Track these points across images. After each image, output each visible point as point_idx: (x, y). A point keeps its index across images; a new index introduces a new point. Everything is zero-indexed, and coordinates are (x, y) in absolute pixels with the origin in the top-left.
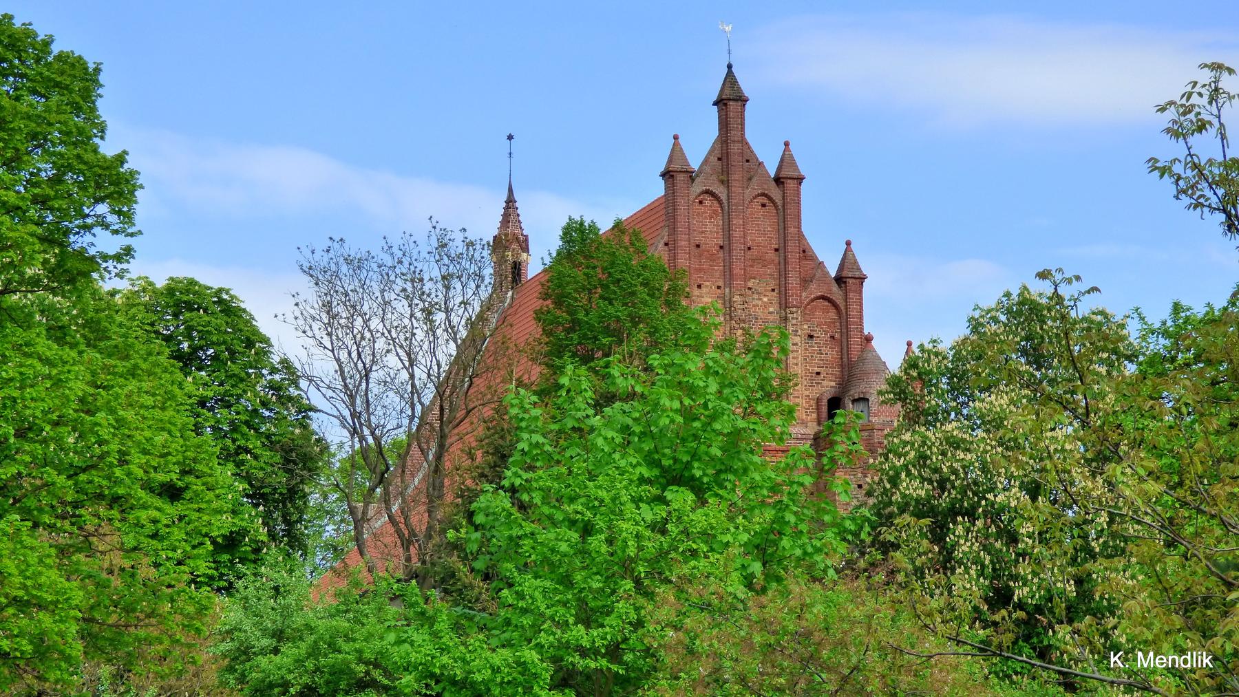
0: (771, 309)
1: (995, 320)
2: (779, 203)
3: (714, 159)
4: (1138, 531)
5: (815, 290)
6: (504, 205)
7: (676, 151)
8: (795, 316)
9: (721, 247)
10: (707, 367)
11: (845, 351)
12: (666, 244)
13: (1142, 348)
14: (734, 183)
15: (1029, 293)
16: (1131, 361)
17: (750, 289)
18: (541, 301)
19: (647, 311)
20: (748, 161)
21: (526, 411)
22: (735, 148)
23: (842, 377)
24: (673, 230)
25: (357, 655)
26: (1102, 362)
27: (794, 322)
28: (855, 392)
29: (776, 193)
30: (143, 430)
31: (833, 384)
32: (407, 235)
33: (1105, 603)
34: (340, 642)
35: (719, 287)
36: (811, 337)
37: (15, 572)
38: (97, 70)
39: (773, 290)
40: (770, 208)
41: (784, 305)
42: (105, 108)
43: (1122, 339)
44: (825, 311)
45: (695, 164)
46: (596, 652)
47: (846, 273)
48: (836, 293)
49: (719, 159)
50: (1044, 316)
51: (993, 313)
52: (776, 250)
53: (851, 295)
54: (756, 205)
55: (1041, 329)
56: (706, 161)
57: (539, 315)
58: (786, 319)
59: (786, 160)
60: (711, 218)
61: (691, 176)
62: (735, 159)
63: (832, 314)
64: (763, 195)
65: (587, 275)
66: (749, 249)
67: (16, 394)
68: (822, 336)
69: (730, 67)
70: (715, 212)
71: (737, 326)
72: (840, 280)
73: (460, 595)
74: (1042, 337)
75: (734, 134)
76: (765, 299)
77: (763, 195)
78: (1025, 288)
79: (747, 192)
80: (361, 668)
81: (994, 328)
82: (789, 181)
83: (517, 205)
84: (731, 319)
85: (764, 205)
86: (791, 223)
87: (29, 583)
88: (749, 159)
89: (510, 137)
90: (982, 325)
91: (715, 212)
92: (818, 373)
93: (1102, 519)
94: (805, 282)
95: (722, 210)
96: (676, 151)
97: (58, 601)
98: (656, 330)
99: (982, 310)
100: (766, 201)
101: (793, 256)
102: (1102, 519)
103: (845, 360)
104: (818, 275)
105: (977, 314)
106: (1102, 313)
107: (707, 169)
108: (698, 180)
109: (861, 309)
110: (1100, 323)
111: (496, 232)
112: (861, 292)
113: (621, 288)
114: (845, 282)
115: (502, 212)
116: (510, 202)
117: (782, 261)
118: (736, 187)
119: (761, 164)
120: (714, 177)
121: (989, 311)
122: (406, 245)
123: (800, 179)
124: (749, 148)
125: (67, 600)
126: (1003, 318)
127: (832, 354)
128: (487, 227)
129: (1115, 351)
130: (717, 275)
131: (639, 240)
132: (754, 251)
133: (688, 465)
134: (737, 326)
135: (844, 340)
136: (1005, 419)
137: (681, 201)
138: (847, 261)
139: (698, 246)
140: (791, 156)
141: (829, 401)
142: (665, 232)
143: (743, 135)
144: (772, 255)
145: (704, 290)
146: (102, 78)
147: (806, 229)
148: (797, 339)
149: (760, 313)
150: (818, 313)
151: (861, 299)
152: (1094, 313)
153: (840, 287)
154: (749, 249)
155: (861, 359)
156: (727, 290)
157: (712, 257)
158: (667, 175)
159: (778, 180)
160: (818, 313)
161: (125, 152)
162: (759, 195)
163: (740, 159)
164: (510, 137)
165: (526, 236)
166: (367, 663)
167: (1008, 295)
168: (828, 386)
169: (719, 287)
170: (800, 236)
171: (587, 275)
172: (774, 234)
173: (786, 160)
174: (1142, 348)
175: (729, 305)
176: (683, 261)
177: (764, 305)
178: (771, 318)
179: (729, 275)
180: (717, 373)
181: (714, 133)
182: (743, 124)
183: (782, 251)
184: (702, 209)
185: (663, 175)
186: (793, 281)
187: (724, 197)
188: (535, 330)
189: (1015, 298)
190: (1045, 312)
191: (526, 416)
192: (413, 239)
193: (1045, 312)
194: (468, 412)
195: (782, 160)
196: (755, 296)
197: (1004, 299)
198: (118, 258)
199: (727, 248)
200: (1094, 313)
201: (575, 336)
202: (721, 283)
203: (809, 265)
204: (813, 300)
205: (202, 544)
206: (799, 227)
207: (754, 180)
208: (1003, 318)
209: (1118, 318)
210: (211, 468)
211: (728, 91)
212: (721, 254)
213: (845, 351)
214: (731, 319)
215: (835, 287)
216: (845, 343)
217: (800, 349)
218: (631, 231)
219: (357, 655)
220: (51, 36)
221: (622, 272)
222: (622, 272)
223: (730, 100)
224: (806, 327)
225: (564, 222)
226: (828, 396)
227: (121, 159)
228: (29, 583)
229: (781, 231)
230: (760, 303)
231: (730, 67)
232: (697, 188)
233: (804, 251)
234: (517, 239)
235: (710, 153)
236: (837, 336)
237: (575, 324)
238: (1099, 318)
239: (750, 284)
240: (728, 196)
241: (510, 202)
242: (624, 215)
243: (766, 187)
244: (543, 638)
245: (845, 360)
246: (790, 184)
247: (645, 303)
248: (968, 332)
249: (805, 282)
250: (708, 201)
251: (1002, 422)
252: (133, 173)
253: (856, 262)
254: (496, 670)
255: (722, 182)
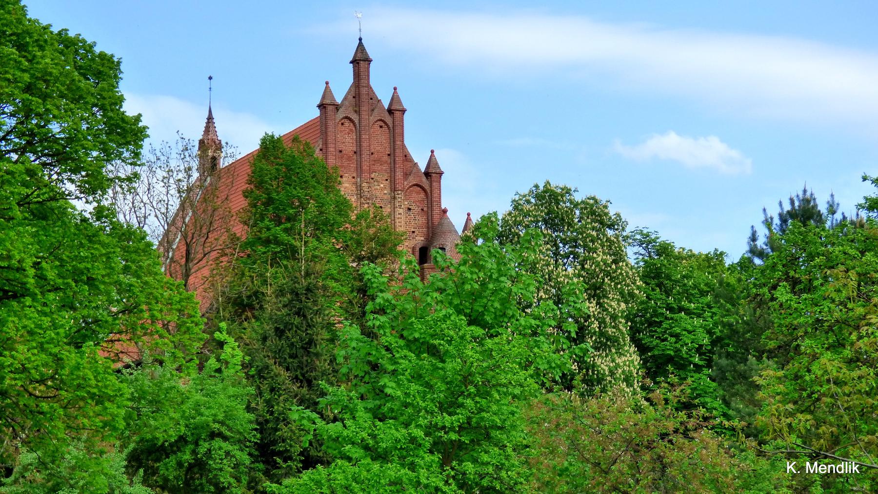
0: (385, 192)
1: (528, 202)
2: (391, 125)
3: (350, 97)
4: (615, 333)
5: (412, 180)
6: (206, 121)
7: (327, 92)
8: (400, 196)
9: (355, 153)
10: (490, 252)
11: (430, 218)
12: (321, 150)
13: (617, 220)
14: (364, 113)
15: (550, 185)
16: (610, 229)
17: (372, 179)
18: (248, 185)
19: (316, 192)
20: (371, 99)
21: (375, 277)
22: (364, 91)
23: (428, 235)
24: (326, 143)
25: (213, 417)
26: (593, 229)
27: (399, 200)
28: (437, 243)
29: (388, 119)
30: (157, 289)
31: (422, 238)
32: (165, 142)
33: (595, 376)
34: (203, 410)
35: (353, 177)
36: (409, 209)
37: (92, 377)
38: (119, 63)
39: (387, 180)
40: (385, 128)
41: (394, 189)
42: (123, 88)
43: (606, 214)
44: (418, 193)
45: (339, 99)
46: (452, 429)
47: (431, 170)
48: (425, 182)
49: (354, 97)
50: (559, 200)
51: (528, 198)
52: (389, 155)
53: (434, 184)
54: (377, 127)
55: (557, 208)
56: (345, 98)
57: (246, 194)
58: (395, 198)
59: (395, 99)
60: (349, 134)
61: (337, 107)
62: (364, 98)
63: (422, 195)
64: (381, 120)
65: (277, 169)
66: (372, 154)
67: (89, 266)
68: (416, 209)
69: (360, 39)
70: (351, 130)
71: (364, 202)
72: (427, 174)
73: (273, 380)
74: (558, 213)
75: (363, 82)
76: (382, 186)
77: (381, 120)
78: (548, 182)
79: (371, 118)
80: (217, 426)
81: (528, 207)
82: (397, 112)
83: (214, 121)
84: (361, 197)
85: (381, 127)
86: (398, 138)
87: (100, 384)
88: (372, 97)
89: (210, 78)
90: (520, 204)
91: (351, 130)
92: (413, 232)
93: (595, 326)
94: (406, 175)
95: (356, 129)
96: (327, 92)
97: (116, 395)
98: (323, 205)
99: (520, 195)
100: (383, 124)
101: (399, 159)
102: (595, 326)
103: (430, 224)
104: (414, 171)
105: (517, 198)
106: (593, 198)
107: (347, 103)
108: (341, 110)
109: (440, 192)
110: (592, 205)
111: (201, 137)
112: (440, 182)
113: (299, 178)
114: (430, 176)
115: (205, 125)
116: (210, 119)
117: (392, 162)
118: (364, 115)
119: (379, 101)
120: (351, 109)
121: (525, 196)
122: (164, 149)
123: (403, 111)
124: (372, 91)
125: (121, 395)
126: (533, 200)
127: (421, 220)
128: (196, 133)
129: (602, 223)
130: (352, 170)
131: (310, 148)
132: (375, 155)
133: (482, 314)
134: (364, 202)
135: (430, 212)
136: (537, 263)
137: (330, 123)
138: (432, 162)
139: (341, 151)
140: (398, 96)
141: (420, 249)
142: (320, 142)
143: (369, 82)
144: (386, 158)
145: (344, 179)
146: (122, 67)
147: (407, 142)
148: (401, 211)
149: (378, 194)
150: (414, 195)
151: (440, 186)
152: (588, 199)
153: (427, 178)
154: (372, 154)
155: (440, 224)
156: (359, 179)
157: (349, 158)
158: (322, 106)
159: (390, 111)
160: (414, 195)
161: (140, 115)
162: (378, 120)
163: (367, 97)
164: (210, 78)
165: (220, 141)
166: (219, 422)
167: (537, 186)
168: (419, 240)
169: (353, 177)
170: (403, 146)
171: (277, 169)
172: (387, 145)
173: (395, 99)
174: (617, 220)
175: (359, 188)
176: (332, 161)
177: (380, 188)
178: (385, 197)
179: (359, 170)
180: (495, 256)
181: (350, 80)
182: (368, 76)
183: (392, 156)
184: (343, 128)
185: (319, 106)
186: (399, 175)
187: (357, 121)
188: (243, 203)
189: (541, 188)
190: (560, 198)
191: (376, 280)
192: (168, 145)
193: (560, 198)
194: (205, 255)
195: (392, 99)
196: (376, 183)
197: (534, 189)
198: (129, 179)
199: (358, 153)
200: (588, 199)
201: (270, 208)
202: (355, 175)
203: (409, 165)
204: (411, 187)
205: (192, 359)
206: (403, 141)
207: (376, 111)
208: (533, 200)
209: (604, 202)
210: (196, 313)
211: (359, 55)
212: (355, 157)
213: (430, 218)
214: (361, 197)
215: (424, 179)
216: (430, 214)
217: (403, 217)
218: (304, 142)
219: (213, 417)
220: (95, 42)
221: (299, 168)
222: (299, 168)
223: (360, 60)
224: (406, 203)
225: (262, 135)
226: (419, 246)
227: (138, 118)
228: (100, 384)
229: (392, 144)
230: (378, 187)
231: (360, 39)
232: (341, 114)
233: (406, 156)
234: (215, 142)
235: (348, 93)
236: (425, 209)
237: (270, 201)
238: (592, 202)
239: (373, 176)
240: (359, 120)
241: (210, 119)
242: (281, 129)
243: (382, 115)
244: (422, 422)
245: (430, 224)
246: (397, 114)
247: (314, 187)
248: (511, 208)
249: (406, 175)
250: (347, 123)
251: (535, 265)
252: (145, 128)
253: (437, 163)
254: (397, 441)
255: (356, 111)
